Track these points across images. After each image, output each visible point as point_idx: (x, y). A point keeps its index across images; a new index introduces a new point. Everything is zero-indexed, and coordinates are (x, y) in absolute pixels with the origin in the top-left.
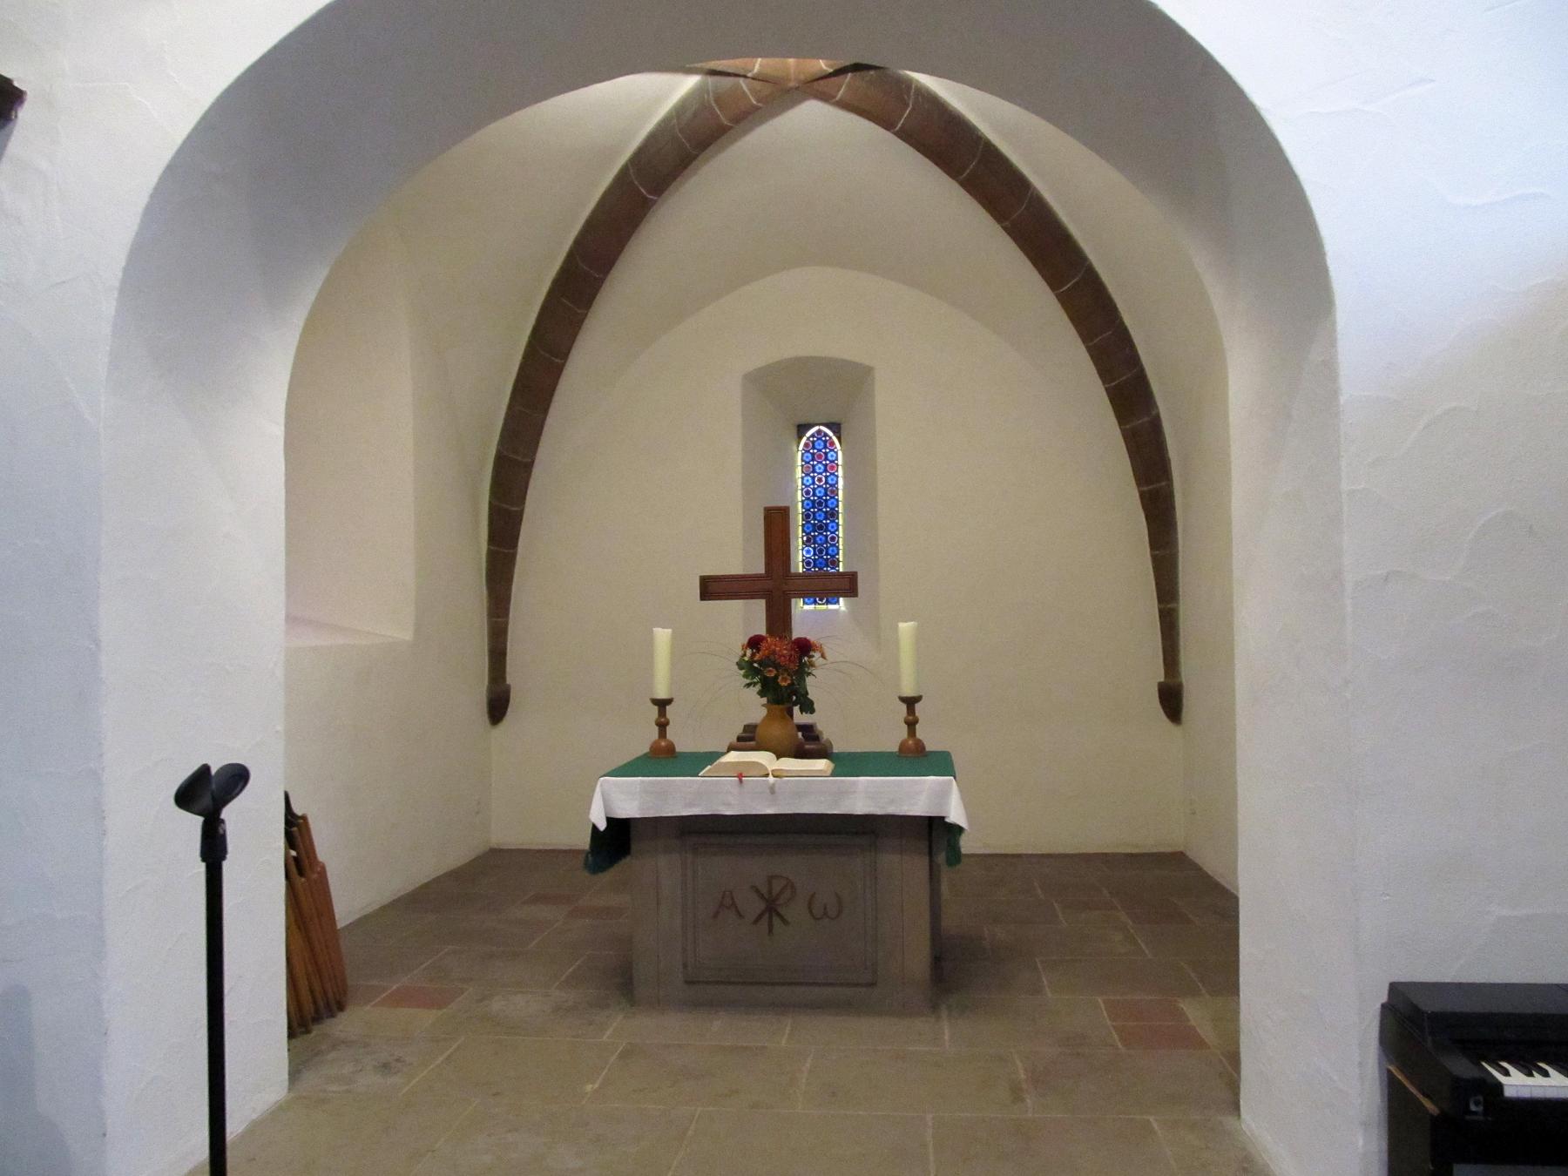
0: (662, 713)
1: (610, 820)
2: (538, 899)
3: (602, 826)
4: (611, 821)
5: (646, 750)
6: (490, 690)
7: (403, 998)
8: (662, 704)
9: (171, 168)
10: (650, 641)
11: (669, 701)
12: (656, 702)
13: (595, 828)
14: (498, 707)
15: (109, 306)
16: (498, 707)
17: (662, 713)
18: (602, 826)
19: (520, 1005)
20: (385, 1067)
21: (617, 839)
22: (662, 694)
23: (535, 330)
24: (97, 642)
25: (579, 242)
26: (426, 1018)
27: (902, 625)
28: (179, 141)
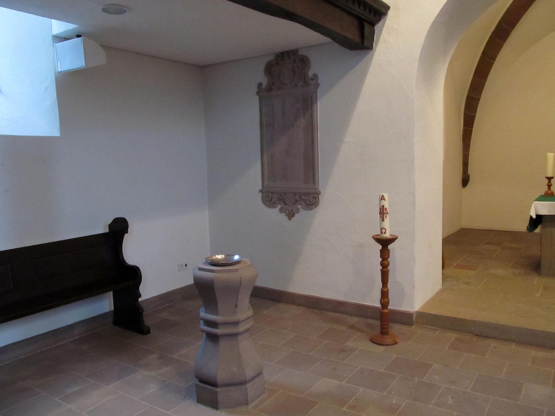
0: (549, 182)
1: (537, 215)
2: (486, 243)
3: (534, 217)
4: (537, 216)
5: (543, 194)
6: (463, 176)
7: (459, 267)
8: (549, 179)
9: (433, 23)
10: (546, 158)
11: (552, 178)
12: (547, 178)
13: (531, 217)
14: (465, 181)
15: (416, 65)
16: (465, 181)
17: (549, 182)
18: (534, 217)
19: (500, 272)
20: (466, 283)
21: (537, 222)
22: (550, 175)
23: (484, 52)
24: (413, 158)
25: (503, 18)
26: (473, 273)
27: (549, 154)
28: (436, 14)
